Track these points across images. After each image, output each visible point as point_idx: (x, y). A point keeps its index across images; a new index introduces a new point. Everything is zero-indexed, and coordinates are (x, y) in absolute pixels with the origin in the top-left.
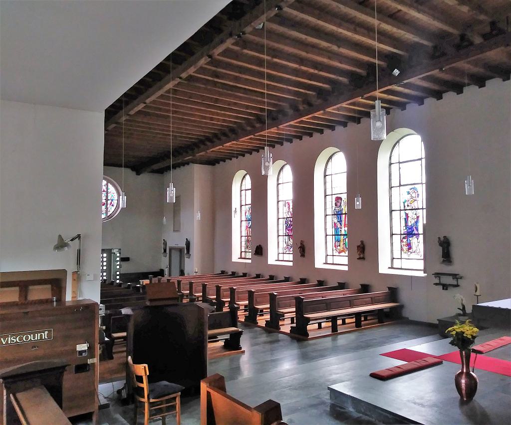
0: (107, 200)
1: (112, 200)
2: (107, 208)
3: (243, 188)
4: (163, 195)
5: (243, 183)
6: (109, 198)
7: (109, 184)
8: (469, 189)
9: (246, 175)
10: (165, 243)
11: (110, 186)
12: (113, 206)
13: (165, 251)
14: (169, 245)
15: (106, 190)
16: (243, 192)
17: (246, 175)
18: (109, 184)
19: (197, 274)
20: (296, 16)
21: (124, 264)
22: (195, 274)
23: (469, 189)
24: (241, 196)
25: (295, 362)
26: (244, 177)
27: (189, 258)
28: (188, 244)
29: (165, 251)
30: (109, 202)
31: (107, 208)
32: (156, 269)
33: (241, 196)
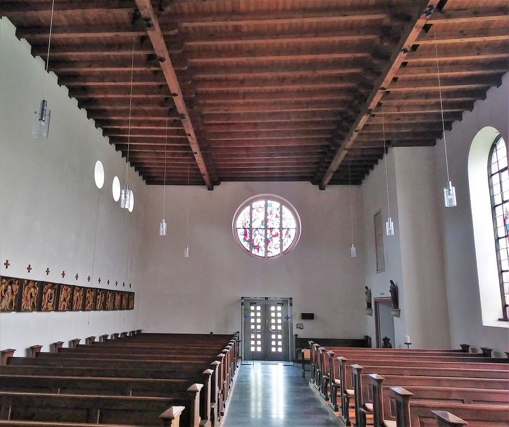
0: (281, 229)
1: (288, 229)
2: (281, 241)
3: (494, 169)
4: (440, 198)
5: (494, 160)
6: (284, 226)
7: (283, 207)
8: (163, 229)
9: (497, 140)
10: (369, 293)
11: (285, 209)
12: (290, 236)
13: (369, 305)
14: (375, 295)
15: (279, 215)
16: (495, 179)
17: (497, 140)
18: (283, 207)
19: (411, 347)
20: (303, 23)
21: (307, 323)
22: (405, 347)
23: (163, 229)
24: (491, 187)
25: (292, 373)
26: (494, 146)
27: (398, 316)
28: (395, 291)
29: (369, 305)
30: (284, 232)
31: (281, 241)
32: (359, 336)
33: (491, 187)
